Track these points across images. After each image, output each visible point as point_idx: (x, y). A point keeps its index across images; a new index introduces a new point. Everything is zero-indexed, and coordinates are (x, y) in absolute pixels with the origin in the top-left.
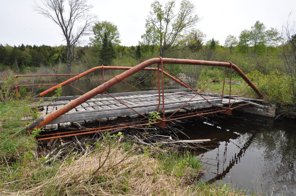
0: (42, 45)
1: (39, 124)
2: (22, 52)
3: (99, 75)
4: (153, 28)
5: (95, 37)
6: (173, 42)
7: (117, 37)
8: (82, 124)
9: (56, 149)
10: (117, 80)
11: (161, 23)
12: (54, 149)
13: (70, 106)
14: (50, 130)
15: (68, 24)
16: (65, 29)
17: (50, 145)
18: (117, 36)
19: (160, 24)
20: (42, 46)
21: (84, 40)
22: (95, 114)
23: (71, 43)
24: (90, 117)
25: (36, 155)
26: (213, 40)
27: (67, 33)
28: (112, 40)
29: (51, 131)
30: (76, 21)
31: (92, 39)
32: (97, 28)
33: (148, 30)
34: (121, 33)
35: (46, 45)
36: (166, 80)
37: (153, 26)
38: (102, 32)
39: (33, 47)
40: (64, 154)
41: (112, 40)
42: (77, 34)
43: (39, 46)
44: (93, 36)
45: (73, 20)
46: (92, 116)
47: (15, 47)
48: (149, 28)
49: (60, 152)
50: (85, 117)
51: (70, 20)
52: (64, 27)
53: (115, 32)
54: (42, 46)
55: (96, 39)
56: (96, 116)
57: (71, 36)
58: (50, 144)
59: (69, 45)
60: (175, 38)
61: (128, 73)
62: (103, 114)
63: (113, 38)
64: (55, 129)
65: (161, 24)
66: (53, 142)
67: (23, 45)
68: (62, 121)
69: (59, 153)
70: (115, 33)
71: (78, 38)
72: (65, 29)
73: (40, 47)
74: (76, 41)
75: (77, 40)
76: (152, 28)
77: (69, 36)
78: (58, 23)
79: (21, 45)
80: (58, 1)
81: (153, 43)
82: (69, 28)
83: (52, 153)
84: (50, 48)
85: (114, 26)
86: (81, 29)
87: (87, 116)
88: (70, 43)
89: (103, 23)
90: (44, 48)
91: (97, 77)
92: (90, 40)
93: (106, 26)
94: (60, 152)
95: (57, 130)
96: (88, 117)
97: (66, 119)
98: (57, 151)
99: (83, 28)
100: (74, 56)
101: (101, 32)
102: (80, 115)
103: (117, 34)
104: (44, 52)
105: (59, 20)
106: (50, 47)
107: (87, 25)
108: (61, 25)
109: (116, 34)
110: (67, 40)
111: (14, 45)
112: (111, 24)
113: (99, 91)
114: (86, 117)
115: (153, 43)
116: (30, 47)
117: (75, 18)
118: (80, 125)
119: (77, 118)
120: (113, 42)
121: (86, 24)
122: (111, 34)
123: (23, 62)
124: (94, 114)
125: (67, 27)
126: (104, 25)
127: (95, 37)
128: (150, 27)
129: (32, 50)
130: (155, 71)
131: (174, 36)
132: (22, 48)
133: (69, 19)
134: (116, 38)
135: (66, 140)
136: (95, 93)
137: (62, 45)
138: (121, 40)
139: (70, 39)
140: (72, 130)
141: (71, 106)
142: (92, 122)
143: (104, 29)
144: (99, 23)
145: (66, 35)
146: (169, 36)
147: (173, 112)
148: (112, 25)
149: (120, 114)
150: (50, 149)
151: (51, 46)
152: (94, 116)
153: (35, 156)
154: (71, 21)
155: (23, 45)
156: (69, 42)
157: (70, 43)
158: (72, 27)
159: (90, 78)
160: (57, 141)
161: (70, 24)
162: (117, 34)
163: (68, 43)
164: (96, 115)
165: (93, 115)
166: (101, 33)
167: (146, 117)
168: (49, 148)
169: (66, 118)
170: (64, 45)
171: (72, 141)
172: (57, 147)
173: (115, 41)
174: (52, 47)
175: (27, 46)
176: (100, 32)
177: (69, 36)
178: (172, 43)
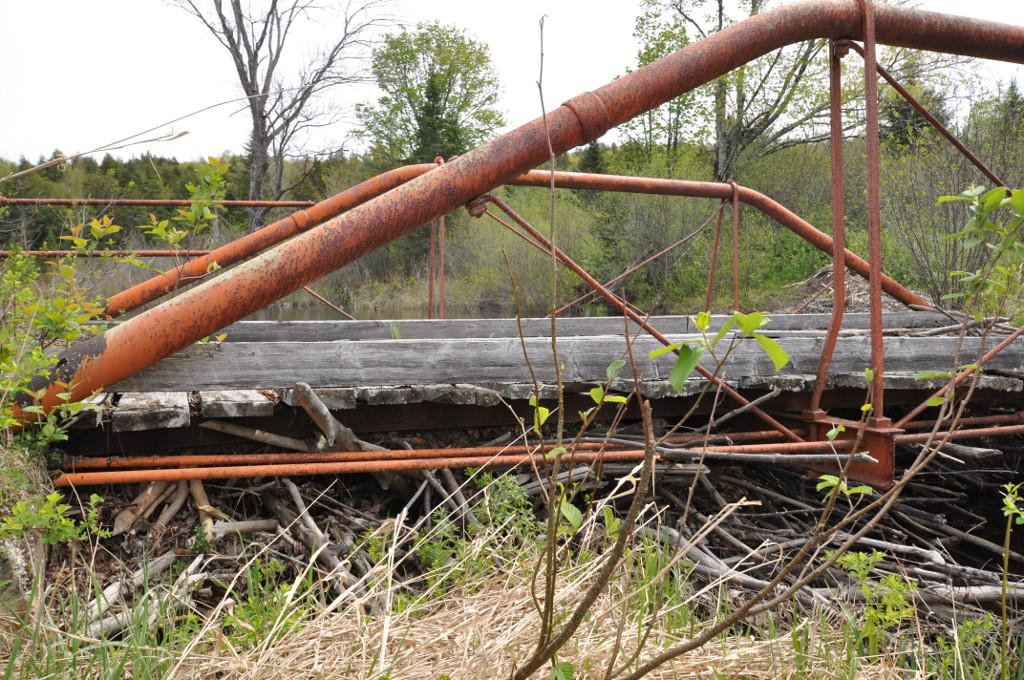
0: (142, 156)
1: (72, 372)
2: (51, 183)
3: (396, 280)
4: (674, 36)
5: (384, 101)
6: (789, 98)
7: (489, 98)
8: (341, 405)
9: (170, 556)
10: (580, 123)
11: (723, 4)
12: (156, 554)
13: (275, 266)
14: (141, 427)
15: (264, 33)
16: (245, 59)
17: (133, 532)
18: (487, 90)
19: (714, 12)
20: (139, 158)
21: (331, 108)
22: (421, 348)
23: (272, 125)
24: (389, 364)
25: (27, 569)
26: (1013, 88)
27: (253, 77)
28: (463, 115)
29: (143, 431)
30: (299, 19)
31: (366, 110)
32: (396, 55)
33: (647, 47)
34: (503, 80)
35: (159, 156)
36: (756, 301)
37: (676, 26)
38: (418, 77)
39: (100, 162)
40: (208, 596)
41: (463, 115)
42: (303, 78)
43: (125, 160)
44: (372, 94)
45: (287, 15)
46: (405, 364)
47: (25, 164)
48: (657, 36)
49: (192, 576)
50: (358, 364)
51: (271, 13)
52: (243, 50)
53: (478, 72)
54: (139, 158)
55: (385, 109)
56: (433, 367)
57: (272, 89)
58: (133, 526)
59: (262, 136)
60: (797, 80)
61: (649, 79)
62: (472, 354)
63: (465, 104)
64: (173, 423)
65: (721, 8)
66: (152, 510)
67: (56, 154)
68: (216, 376)
69: (183, 576)
70: (480, 77)
71: (303, 99)
72: (245, 59)
73: (131, 166)
74: (295, 115)
75: (301, 105)
76: (668, 36)
77: (266, 89)
78: (219, 27)
79: (48, 156)
80: (219, 5)
81: (674, 115)
82: (263, 52)
83: (138, 577)
84: (172, 167)
85: (471, 43)
86: (321, 57)
87: (377, 356)
88: (264, 124)
89: (423, 31)
90: (146, 165)
91: (384, 288)
92: (360, 117)
93: (439, 46)
94: (192, 576)
95: (184, 427)
96: (380, 364)
97: (244, 367)
98: (172, 572)
99: (328, 55)
100: (279, 187)
101: (411, 75)
102: (330, 347)
103: (489, 83)
104: (147, 183)
105: (223, 19)
106: (174, 163)
107: (349, 40)
108: (230, 38)
109: (481, 83)
110: (254, 112)
111: (22, 156)
112: (462, 38)
113: (459, 182)
114: (366, 364)
115: (674, 115)
116: (88, 165)
117: (293, 9)
118: (325, 410)
119: (310, 366)
120: (465, 125)
121: (346, 35)
122: (460, 82)
123: (51, 232)
124: (415, 347)
125: (258, 47)
126: (428, 42)
127: (384, 101)
128: (658, 31)
129: (96, 176)
130: (731, 200)
131: (795, 69)
132: (52, 171)
133: (269, 10)
134: (483, 104)
135: (230, 496)
136: (433, 196)
137: (228, 152)
138: (504, 111)
139: (268, 107)
140: (277, 449)
141: (281, 268)
142: (402, 400)
143: (425, 61)
144: (404, 35)
145: (250, 87)
146: (764, 72)
147: (931, 385)
148: (467, 42)
149: (583, 370)
150: (130, 556)
151: (180, 160)
152: (419, 365)
153: (22, 571)
154: (279, 20)
155: (56, 154)
156: (264, 118)
157: (268, 124)
158: (279, 50)
159: (351, 294)
160: (180, 511)
161: (271, 32)
162: (489, 83)
163: (256, 124)
164: (432, 358)
165: (409, 354)
166: (411, 81)
167: (749, 405)
168: (124, 544)
169: (245, 360)
170: (238, 154)
171: (273, 522)
172: (172, 545)
173: (479, 118)
174: (185, 163)
175: (76, 160)
176: (406, 77)
177: (266, 89)
178: (785, 103)
